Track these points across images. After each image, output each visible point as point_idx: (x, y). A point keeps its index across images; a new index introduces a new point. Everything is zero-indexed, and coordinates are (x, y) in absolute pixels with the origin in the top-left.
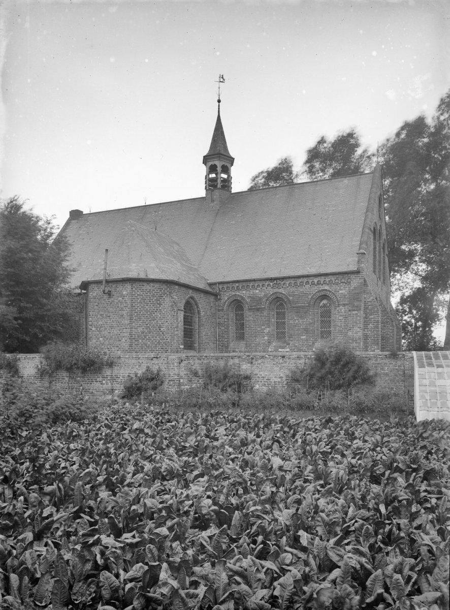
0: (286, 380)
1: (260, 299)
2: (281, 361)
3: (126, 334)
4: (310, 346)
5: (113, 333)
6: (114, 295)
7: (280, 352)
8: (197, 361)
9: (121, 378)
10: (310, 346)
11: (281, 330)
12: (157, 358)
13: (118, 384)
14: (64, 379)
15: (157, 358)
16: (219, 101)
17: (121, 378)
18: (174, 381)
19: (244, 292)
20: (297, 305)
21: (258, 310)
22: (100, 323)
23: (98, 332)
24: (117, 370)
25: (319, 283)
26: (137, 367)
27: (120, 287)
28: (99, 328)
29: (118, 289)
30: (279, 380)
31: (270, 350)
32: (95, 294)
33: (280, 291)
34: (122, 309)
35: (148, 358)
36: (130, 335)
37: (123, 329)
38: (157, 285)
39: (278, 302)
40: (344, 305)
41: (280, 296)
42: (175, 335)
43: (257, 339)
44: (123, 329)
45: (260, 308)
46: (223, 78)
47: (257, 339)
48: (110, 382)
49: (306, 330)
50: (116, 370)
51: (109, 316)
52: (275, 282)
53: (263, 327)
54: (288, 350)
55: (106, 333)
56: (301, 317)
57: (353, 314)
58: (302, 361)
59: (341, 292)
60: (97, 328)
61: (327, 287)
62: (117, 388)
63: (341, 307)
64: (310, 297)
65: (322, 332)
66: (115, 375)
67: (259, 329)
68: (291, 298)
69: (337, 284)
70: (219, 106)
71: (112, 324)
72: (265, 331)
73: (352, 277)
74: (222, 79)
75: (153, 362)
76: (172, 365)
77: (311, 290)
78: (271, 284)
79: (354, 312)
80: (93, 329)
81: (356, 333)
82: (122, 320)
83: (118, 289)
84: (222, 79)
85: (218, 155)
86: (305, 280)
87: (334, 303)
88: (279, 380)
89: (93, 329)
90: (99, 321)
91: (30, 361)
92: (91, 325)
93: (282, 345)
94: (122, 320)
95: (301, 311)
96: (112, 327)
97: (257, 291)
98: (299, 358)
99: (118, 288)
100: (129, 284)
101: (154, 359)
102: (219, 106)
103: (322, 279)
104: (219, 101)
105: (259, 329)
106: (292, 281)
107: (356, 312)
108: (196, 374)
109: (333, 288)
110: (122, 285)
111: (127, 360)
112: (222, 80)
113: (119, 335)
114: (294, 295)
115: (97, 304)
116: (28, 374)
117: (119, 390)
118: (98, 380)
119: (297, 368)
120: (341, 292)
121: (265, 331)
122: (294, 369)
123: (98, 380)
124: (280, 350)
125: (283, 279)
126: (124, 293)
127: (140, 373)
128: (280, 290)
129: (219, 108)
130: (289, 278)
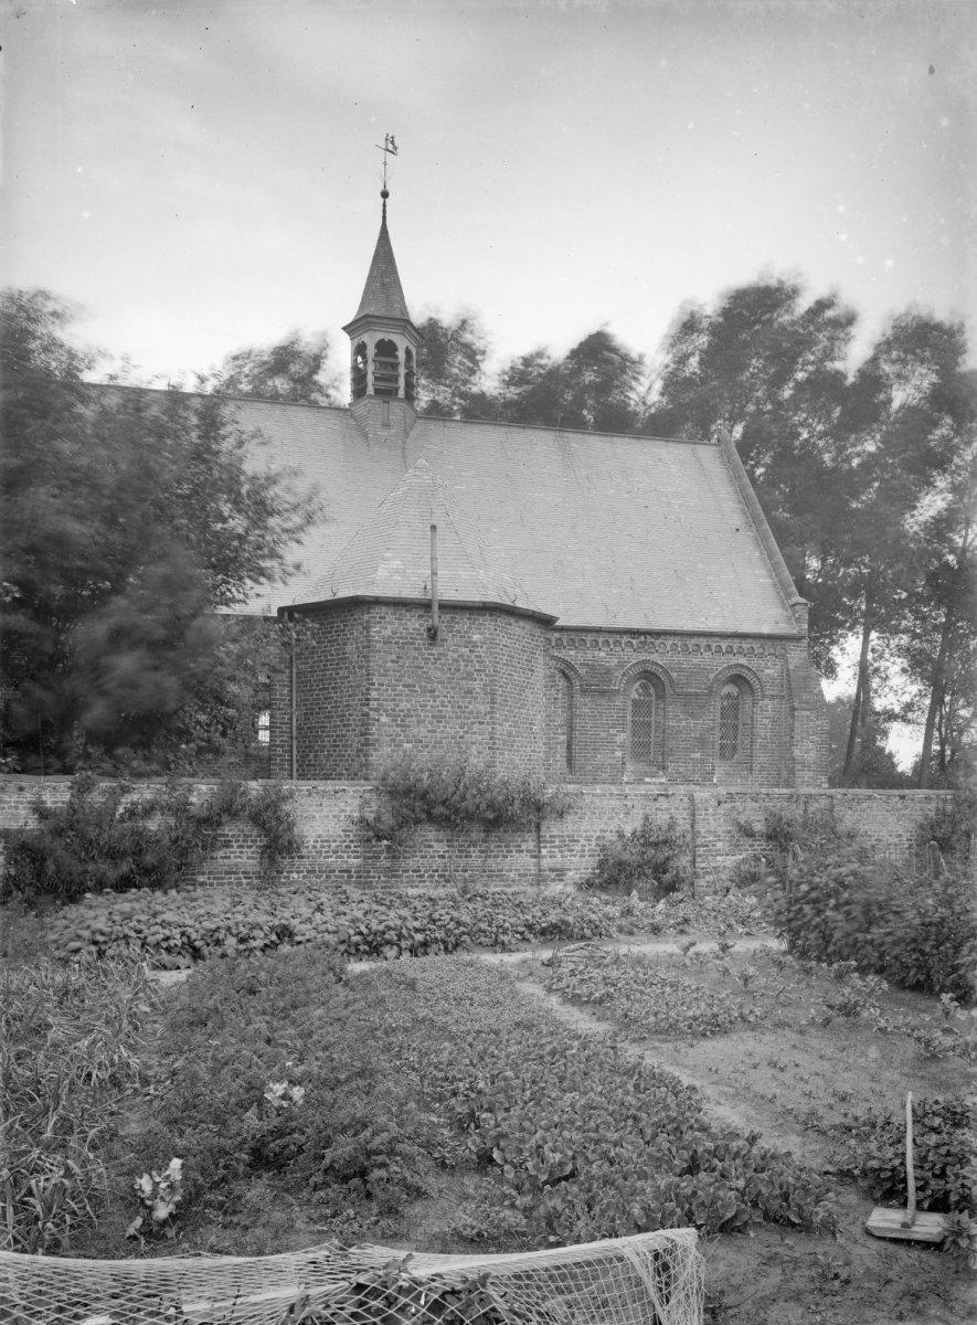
0: (908, 840)
1: (608, 671)
2: (899, 805)
3: (480, 738)
4: (708, 774)
5: (443, 732)
6: (446, 640)
7: (650, 783)
8: (750, 804)
9: (582, 841)
10: (708, 774)
11: (641, 740)
12: (667, 796)
13: (575, 856)
14: (430, 846)
15: (667, 796)
16: (385, 195)
17: (582, 841)
18: (707, 846)
19: (572, 653)
20: (685, 690)
21: (602, 693)
22: (404, 705)
23: (398, 729)
24: (574, 823)
25: (730, 651)
26: (622, 816)
27: (463, 623)
28: (402, 720)
29: (457, 627)
30: (896, 840)
31: (625, 779)
32: (388, 632)
33: (654, 657)
34: (469, 677)
35: (646, 795)
36: (491, 738)
37: (473, 723)
38: (528, 626)
39: (650, 677)
40: (772, 697)
41: (653, 669)
42: (557, 743)
43: (599, 756)
44: (473, 723)
45: (608, 691)
46: (393, 143)
47: (599, 756)
48: (561, 852)
49: (702, 742)
50: (570, 825)
51: (432, 691)
52: (642, 638)
53: (612, 731)
54: (664, 780)
55: (422, 731)
56: (692, 716)
57: (802, 716)
58: (932, 806)
59: (768, 671)
60: (393, 715)
61: (743, 661)
62: (572, 866)
63: (767, 701)
64: (712, 676)
65: (722, 747)
66: (568, 836)
67: (603, 735)
68: (674, 675)
69: (761, 656)
70: (384, 206)
71: (441, 711)
72: (617, 739)
73: (790, 645)
74: (391, 146)
75: (658, 805)
76: (703, 813)
77: (717, 663)
78: (634, 642)
79: (804, 713)
80: (384, 719)
81: (807, 752)
82: (469, 702)
83: (457, 627)
84: (391, 146)
85: (365, 321)
86: (703, 642)
87: (753, 692)
88: (896, 840)
89: (384, 719)
90: (401, 701)
91: (325, 802)
92: (376, 710)
93: (647, 769)
94: (469, 702)
95: (693, 702)
96: (439, 718)
97: (603, 654)
98: (928, 799)
99: (458, 623)
100: (487, 617)
101: (660, 799)
102: (384, 206)
103: (736, 644)
104: (385, 195)
105: (603, 735)
106: (677, 640)
107: (808, 713)
108: (748, 833)
109: (754, 663)
110: (468, 619)
111: (597, 801)
112: (390, 147)
113: (461, 737)
114: (681, 670)
115: (394, 657)
116: (320, 836)
117: (581, 865)
118: (523, 848)
119: (926, 817)
120: (768, 671)
121: (617, 739)
122: (920, 819)
123: (523, 848)
124: (647, 780)
125: (658, 634)
126: (476, 637)
127: (628, 830)
128: (652, 656)
129: (384, 211)
130: (674, 634)
